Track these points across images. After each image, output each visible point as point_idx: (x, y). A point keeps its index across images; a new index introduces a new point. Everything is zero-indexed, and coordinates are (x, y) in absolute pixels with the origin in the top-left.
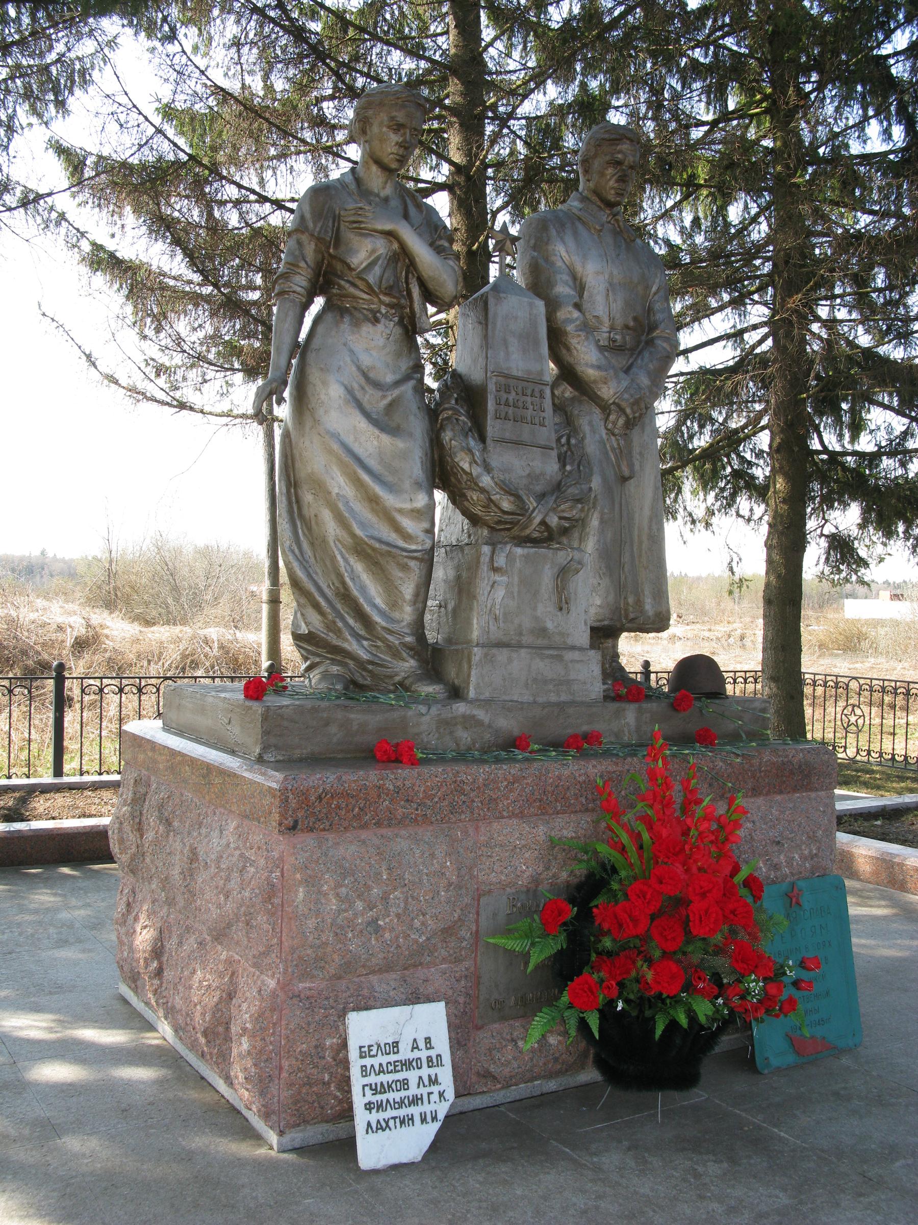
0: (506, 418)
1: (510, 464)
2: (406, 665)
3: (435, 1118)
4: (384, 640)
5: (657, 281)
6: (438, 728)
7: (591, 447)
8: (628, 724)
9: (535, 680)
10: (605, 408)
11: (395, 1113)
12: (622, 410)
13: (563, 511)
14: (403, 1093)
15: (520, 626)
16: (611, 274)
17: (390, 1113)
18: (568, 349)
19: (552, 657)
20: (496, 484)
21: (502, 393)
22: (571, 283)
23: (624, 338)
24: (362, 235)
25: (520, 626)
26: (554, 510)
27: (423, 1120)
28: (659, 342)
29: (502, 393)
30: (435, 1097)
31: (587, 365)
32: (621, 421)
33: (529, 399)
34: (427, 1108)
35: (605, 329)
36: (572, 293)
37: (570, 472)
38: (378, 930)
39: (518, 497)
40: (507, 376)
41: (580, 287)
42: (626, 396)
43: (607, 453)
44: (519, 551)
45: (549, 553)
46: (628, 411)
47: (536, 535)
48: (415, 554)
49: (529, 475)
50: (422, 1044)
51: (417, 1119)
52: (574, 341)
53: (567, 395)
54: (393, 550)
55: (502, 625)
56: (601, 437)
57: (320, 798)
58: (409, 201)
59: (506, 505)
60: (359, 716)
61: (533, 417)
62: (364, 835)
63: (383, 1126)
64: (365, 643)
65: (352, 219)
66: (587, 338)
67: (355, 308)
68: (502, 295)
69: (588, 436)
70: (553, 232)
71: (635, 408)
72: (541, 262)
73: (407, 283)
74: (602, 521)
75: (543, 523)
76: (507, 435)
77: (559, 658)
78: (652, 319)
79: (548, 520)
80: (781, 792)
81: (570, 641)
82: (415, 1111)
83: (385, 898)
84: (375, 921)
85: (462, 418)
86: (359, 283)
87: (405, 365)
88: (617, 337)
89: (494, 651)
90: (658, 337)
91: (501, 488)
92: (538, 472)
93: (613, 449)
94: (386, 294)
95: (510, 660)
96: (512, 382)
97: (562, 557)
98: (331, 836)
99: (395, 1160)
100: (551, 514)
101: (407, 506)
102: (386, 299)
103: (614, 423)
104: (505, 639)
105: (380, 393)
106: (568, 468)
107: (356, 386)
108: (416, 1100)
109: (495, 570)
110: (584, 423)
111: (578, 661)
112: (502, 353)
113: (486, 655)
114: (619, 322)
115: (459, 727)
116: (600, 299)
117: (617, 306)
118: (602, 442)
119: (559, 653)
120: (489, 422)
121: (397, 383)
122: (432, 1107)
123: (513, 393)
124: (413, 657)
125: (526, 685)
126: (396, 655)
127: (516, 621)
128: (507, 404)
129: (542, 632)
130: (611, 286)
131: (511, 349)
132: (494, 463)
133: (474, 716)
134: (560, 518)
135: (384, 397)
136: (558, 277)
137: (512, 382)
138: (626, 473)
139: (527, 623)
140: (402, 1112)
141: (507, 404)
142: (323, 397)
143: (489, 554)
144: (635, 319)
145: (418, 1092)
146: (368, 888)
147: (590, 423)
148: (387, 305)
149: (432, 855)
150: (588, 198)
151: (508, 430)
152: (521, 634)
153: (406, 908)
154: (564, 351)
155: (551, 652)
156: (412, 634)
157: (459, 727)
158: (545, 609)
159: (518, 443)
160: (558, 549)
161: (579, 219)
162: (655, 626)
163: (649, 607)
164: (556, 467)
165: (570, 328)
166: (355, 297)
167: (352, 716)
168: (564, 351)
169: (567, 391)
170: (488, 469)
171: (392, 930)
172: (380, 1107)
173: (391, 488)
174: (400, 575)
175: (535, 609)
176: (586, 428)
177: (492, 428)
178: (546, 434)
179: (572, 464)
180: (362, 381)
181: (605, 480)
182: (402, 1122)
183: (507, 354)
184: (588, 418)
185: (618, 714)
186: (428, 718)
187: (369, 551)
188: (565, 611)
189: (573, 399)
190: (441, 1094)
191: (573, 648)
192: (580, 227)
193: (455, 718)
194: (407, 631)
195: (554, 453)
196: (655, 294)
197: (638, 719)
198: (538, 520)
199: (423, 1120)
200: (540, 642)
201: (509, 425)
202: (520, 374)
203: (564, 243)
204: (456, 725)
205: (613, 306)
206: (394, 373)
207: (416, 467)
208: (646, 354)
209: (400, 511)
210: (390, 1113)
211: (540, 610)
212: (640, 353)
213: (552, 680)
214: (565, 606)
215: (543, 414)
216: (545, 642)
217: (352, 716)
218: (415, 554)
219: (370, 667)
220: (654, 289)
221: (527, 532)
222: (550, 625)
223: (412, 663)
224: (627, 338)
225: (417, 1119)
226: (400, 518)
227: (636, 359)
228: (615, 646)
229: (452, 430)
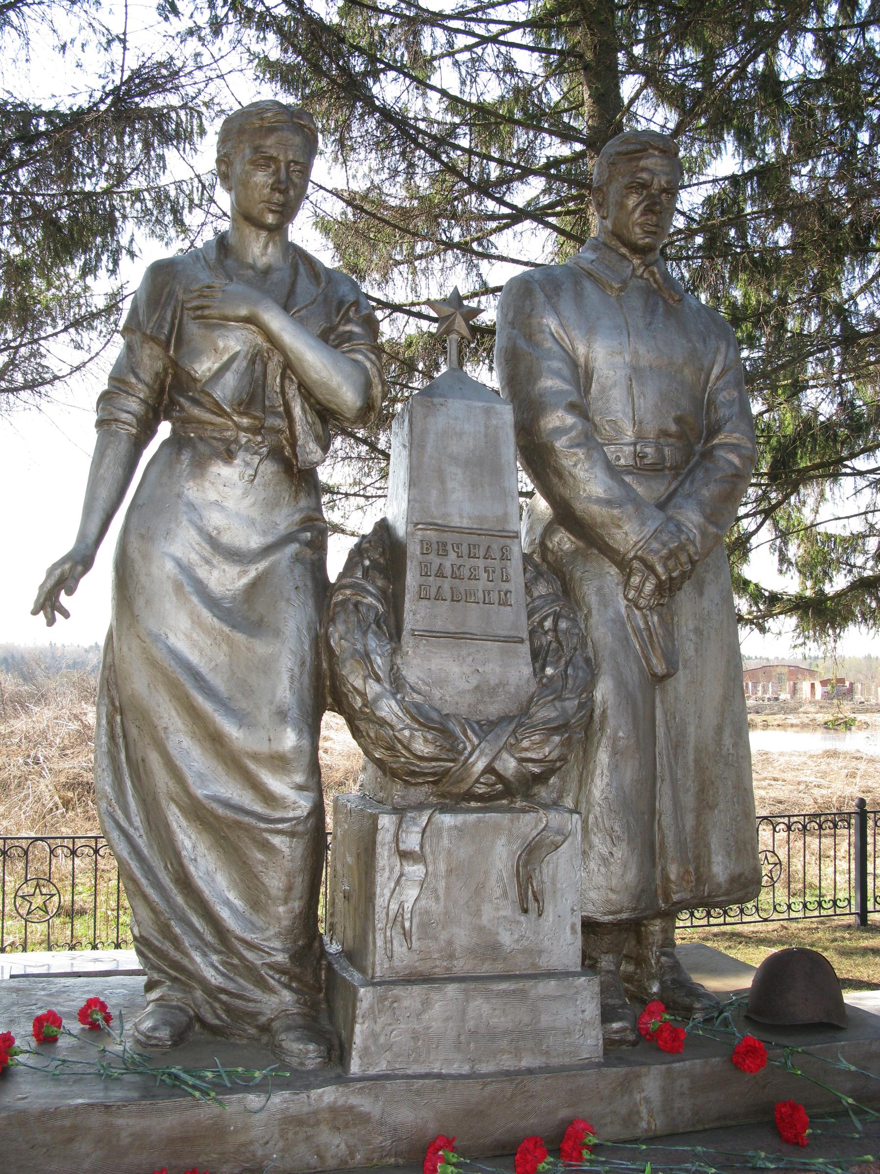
1: (455, 668)
2: (274, 1000)
4: (242, 958)
5: (720, 358)
6: (283, 1133)
7: (601, 632)
8: (647, 1100)
9: (473, 1033)
10: (623, 565)
12: (651, 569)
13: (526, 750)
15: (450, 943)
16: (636, 352)
18: (560, 476)
19: (506, 993)
20: (407, 711)
21: (432, 557)
22: (566, 372)
23: (659, 450)
24: (208, 326)
25: (450, 943)
26: (510, 748)
28: (721, 453)
29: (432, 557)
31: (589, 498)
32: (649, 587)
33: (481, 563)
35: (628, 440)
36: (566, 387)
37: (551, 678)
39: (444, 732)
40: (441, 528)
41: (581, 376)
42: (655, 545)
43: (627, 639)
44: (447, 820)
45: (504, 819)
46: (660, 569)
47: (481, 790)
48: (280, 826)
49: (477, 687)
52: (567, 463)
53: (567, 546)
54: (247, 819)
55: (416, 944)
56: (618, 613)
58: (302, 269)
59: (421, 747)
60: (131, 1121)
61: (487, 592)
64: (215, 958)
65: (195, 303)
66: (589, 457)
67: (201, 439)
68: (436, 400)
69: (594, 612)
70: (540, 297)
71: (671, 563)
72: (522, 343)
73: (283, 393)
74: (615, 753)
75: (490, 769)
76: (439, 625)
77: (522, 995)
78: (713, 417)
79: (498, 765)
81: (544, 963)
85: (370, 600)
86: (205, 400)
87: (285, 519)
88: (648, 450)
89: (398, 991)
90: (722, 445)
91: (413, 718)
92: (493, 681)
93: (637, 631)
94: (241, 414)
95: (426, 1004)
96: (448, 537)
97: (529, 824)
100: (505, 755)
101: (263, 748)
102: (245, 421)
103: (639, 590)
104: (424, 967)
105: (238, 569)
106: (549, 671)
107: (194, 557)
109: (405, 855)
110: (589, 592)
111: (555, 998)
112: (434, 493)
113: (382, 999)
114: (651, 429)
115: (324, 1128)
116: (618, 395)
117: (647, 402)
118: (619, 622)
119: (520, 985)
120: (407, 605)
121: (267, 550)
123: (452, 555)
124: (287, 987)
125: (458, 1046)
126: (261, 983)
127: (444, 936)
128: (440, 574)
129: (491, 949)
130: (636, 373)
131: (450, 485)
132: (412, 674)
133: (351, 1108)
134: (522, 760)
135: (245, 572)
136: (545, 364)
137: (448, 537)
138: (660, 668)
139: (462, 937)
141: (440, 574)
142: (143, 579)
143: (392, 829)
144: (678, 420)
147: (600, 591)
148: (246, 430)
150: (605, 244)
151: (443, 616)
152: (452, 957)
154: (555, 480)
155: (504, 986)
156: (283, 951)
157: (324, 1128)
158: (498, 911)
159: (457, 636)
160: (523, 811)
161: (590, 275)
162: (735, 896)
163: (720, 869)
164: (527, 670)
165: (560, 444)
166: (200, 422)
167: (120, 1121)
168: (555, 480)
169: (563, 541)
170: (397, 684)
173: (242, 719)
174: (260, 856)
175: (478, 913)
176: (593, 600)
177: (415, 614)
178: (512, 618)
179: (555, 665)
180: (207, 550)
181: (620, 684)
183: (444, 492)
184: (596, 583)
185: (626, 1086)
186: (263, 1116)
187: (211, 819)
188: (533, 915)
189: (576, 552)
191: (550, 974)
192: (588, 285)
193: (315, 1113)
194: (277, 944)
195: (525, 648)
196: (718, 378)
197: (665, 1091)
198: (480, 766)
200: (486, 968)
201: (443, 608)
202: (465, 523)
203: (557, 313)
204: (317, 1123)
205: (640, 402)
206: (265, 533)
207: (284, 686)
208: (700, 474)
212: (691, 471)
213: (505, 1033)
214: (532, 905)
215: (506, 586)
216: (499, 968)
217: (120, 1121)
218: (280, 826)
219: (223, 997)
220: (716, 371)
221: (464, 787)
222: (506, 939)
223: (287, 996)
224: (667, 451)
226: (252, 766)
227: (682, 484)
229: (345, 622)
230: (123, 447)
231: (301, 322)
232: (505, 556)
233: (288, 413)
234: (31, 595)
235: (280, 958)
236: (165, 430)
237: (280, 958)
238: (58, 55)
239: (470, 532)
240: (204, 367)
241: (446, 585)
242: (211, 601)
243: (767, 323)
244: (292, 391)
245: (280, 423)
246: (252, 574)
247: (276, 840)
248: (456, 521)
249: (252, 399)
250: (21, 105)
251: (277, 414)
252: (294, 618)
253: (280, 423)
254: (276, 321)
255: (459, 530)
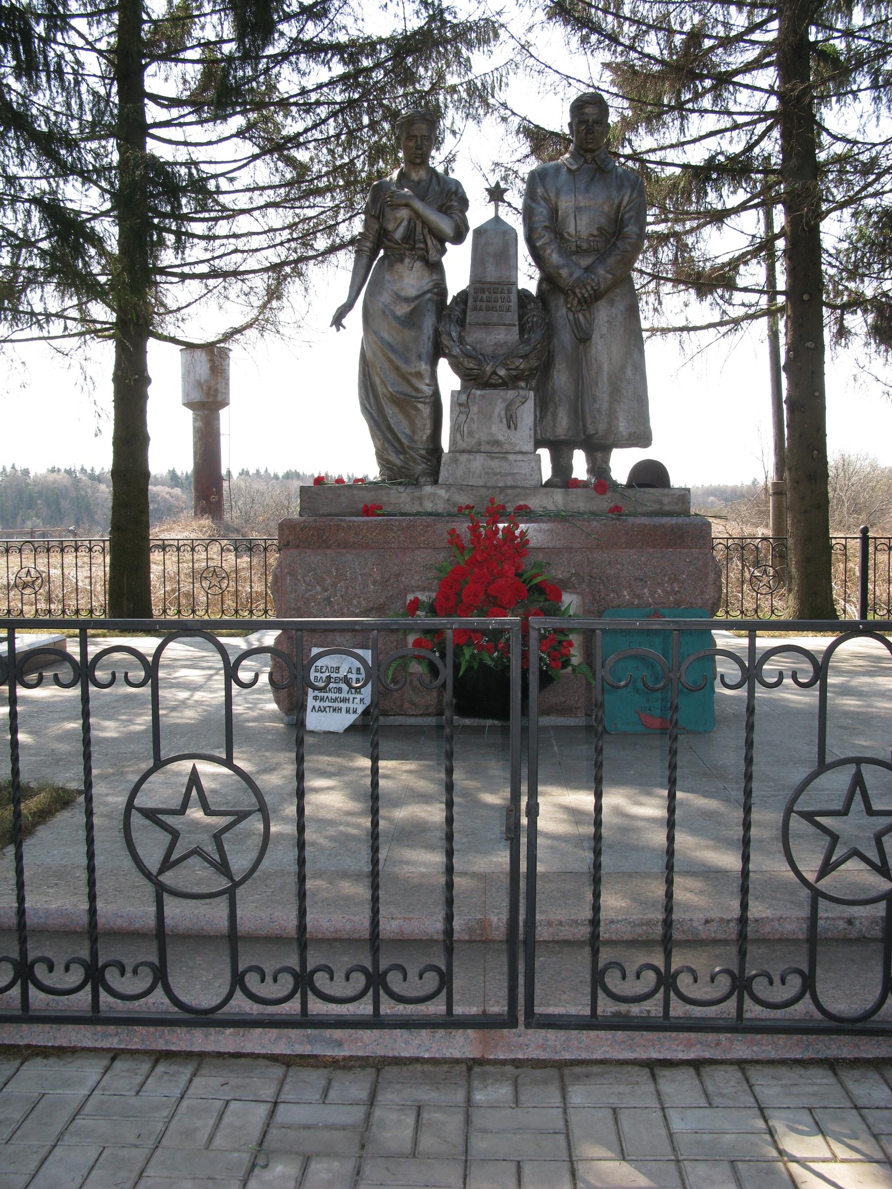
0: (481, 310)
3: (355, 712)
11: (331, 704)
14: (337, 695)
17: (327, 704)
27: (348, 711)
30: (357, 701)
32: (576, 302)
34: (351, 705)
38: (330, 603)
40: (484, 283)
45: (502, 393)
50: (354, 671)
51: (344, 710)
57: (302, 529)
62: (328, 552)
63: (321, 710)
77: (505, 459)
80: (654, 547)
82: (344, 706)
83: (334, 585)
84: (329, 598)
98: (309, 551)
99: (327, 729)
101: (413, 370)
108: (344, 700)
122: (355, 706)
140: (335, 705)
145: (347, 696)
146: (324, 580)
149: (366, 564)
153: (346, 592)
171: (339, 604)
172: (322, 699)
182: (334, 710)
190: (361, 700)
196: (628, 204)
199: (348, 711)
209: (410, 374)
210: (327, 704)
211: (494, 428)
214: (512, 426)
225: (344, 710)
226: (410, 378)
228: (606, 461)
230: (365, 261)
231: (429, 204)
232: (509, 292)
233: (425, 243)
234: (332, 312)
235: (423, 452)
236: (382, 253)
237: (423, 452)
238: (382, 13)
239: (494, 283)
240: (390, 227)
241: (484, 304)
242: (396, 318)
243: (91, 257)
244: (426, 231)
245: (422, 246)
246: (413, 305)
247: (420, 406)
248: (489, 280)
249: (410, 235)
250: (368, 38)
251: (420, 242)
252: (429, 323)
253: (422, 246)
254: (418, 205)
255: (490, 283)
